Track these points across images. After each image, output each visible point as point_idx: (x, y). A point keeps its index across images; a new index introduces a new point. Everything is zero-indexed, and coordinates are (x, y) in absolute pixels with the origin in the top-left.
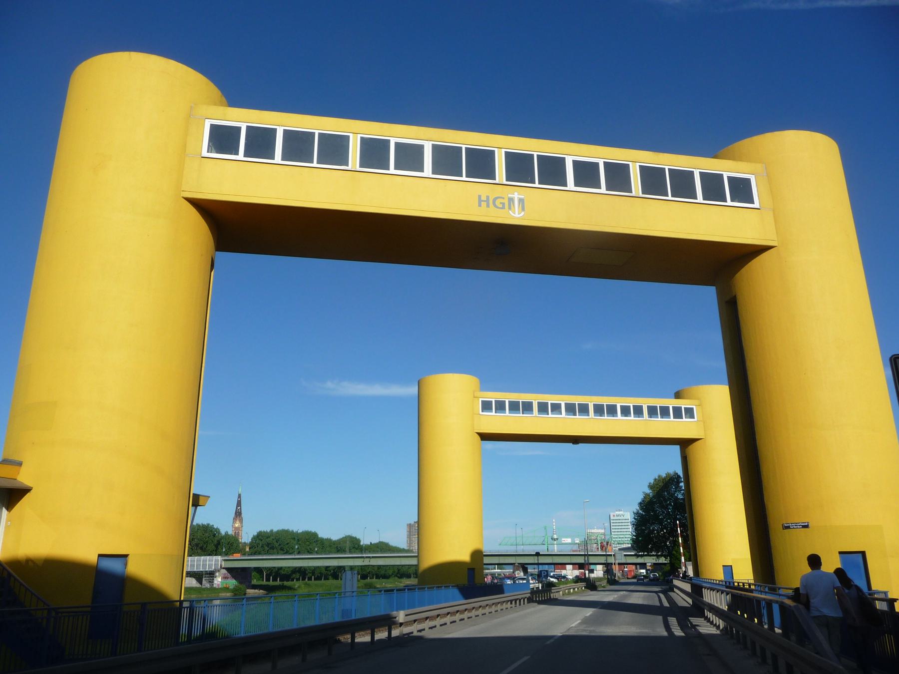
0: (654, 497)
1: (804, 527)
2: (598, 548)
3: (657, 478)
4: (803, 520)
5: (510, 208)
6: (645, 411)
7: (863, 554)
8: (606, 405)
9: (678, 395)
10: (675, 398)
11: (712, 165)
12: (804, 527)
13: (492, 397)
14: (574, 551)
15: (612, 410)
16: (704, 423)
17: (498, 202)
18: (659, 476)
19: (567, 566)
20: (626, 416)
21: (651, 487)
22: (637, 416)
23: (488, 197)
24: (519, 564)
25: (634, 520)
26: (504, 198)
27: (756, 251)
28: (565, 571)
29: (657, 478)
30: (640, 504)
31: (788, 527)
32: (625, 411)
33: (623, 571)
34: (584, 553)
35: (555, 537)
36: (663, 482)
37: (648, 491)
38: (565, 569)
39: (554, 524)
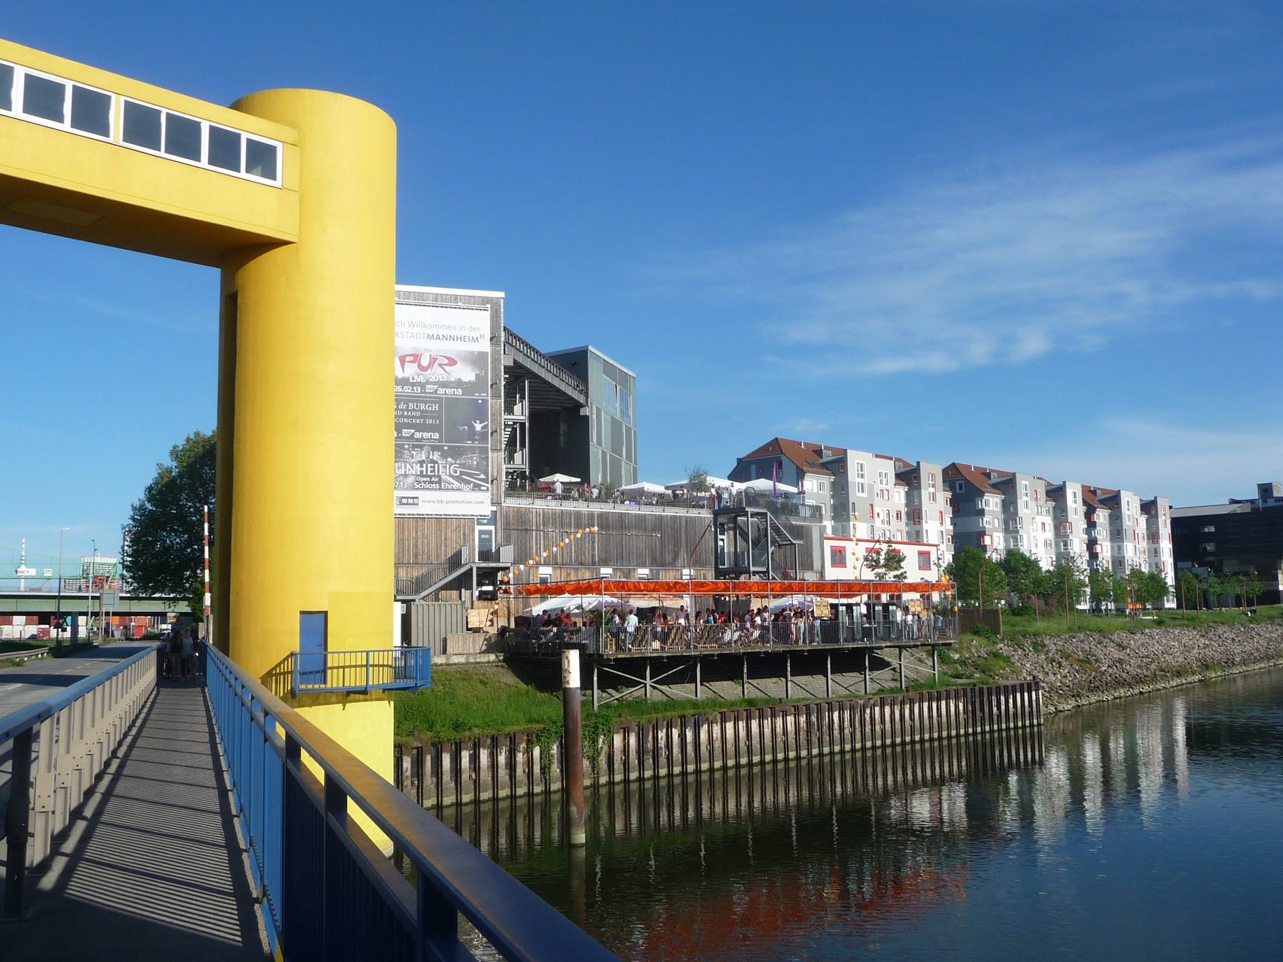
0: (180, 475)
2: (88, 587)
3: (192, 436)
6: (117, 116)
14: (32, 590)
16: (301, 198)
18: (197, 434)
19: (14, 617)
21: (175, 453)
25: (131, 522)
28: (11, 626)
29: (192, 436)
30: (150, 489)
33: (125, 627)
34: (57, 594)
36: (204, 446)
37: (170, 463)
38: (10, 623)
39: (24, 546)
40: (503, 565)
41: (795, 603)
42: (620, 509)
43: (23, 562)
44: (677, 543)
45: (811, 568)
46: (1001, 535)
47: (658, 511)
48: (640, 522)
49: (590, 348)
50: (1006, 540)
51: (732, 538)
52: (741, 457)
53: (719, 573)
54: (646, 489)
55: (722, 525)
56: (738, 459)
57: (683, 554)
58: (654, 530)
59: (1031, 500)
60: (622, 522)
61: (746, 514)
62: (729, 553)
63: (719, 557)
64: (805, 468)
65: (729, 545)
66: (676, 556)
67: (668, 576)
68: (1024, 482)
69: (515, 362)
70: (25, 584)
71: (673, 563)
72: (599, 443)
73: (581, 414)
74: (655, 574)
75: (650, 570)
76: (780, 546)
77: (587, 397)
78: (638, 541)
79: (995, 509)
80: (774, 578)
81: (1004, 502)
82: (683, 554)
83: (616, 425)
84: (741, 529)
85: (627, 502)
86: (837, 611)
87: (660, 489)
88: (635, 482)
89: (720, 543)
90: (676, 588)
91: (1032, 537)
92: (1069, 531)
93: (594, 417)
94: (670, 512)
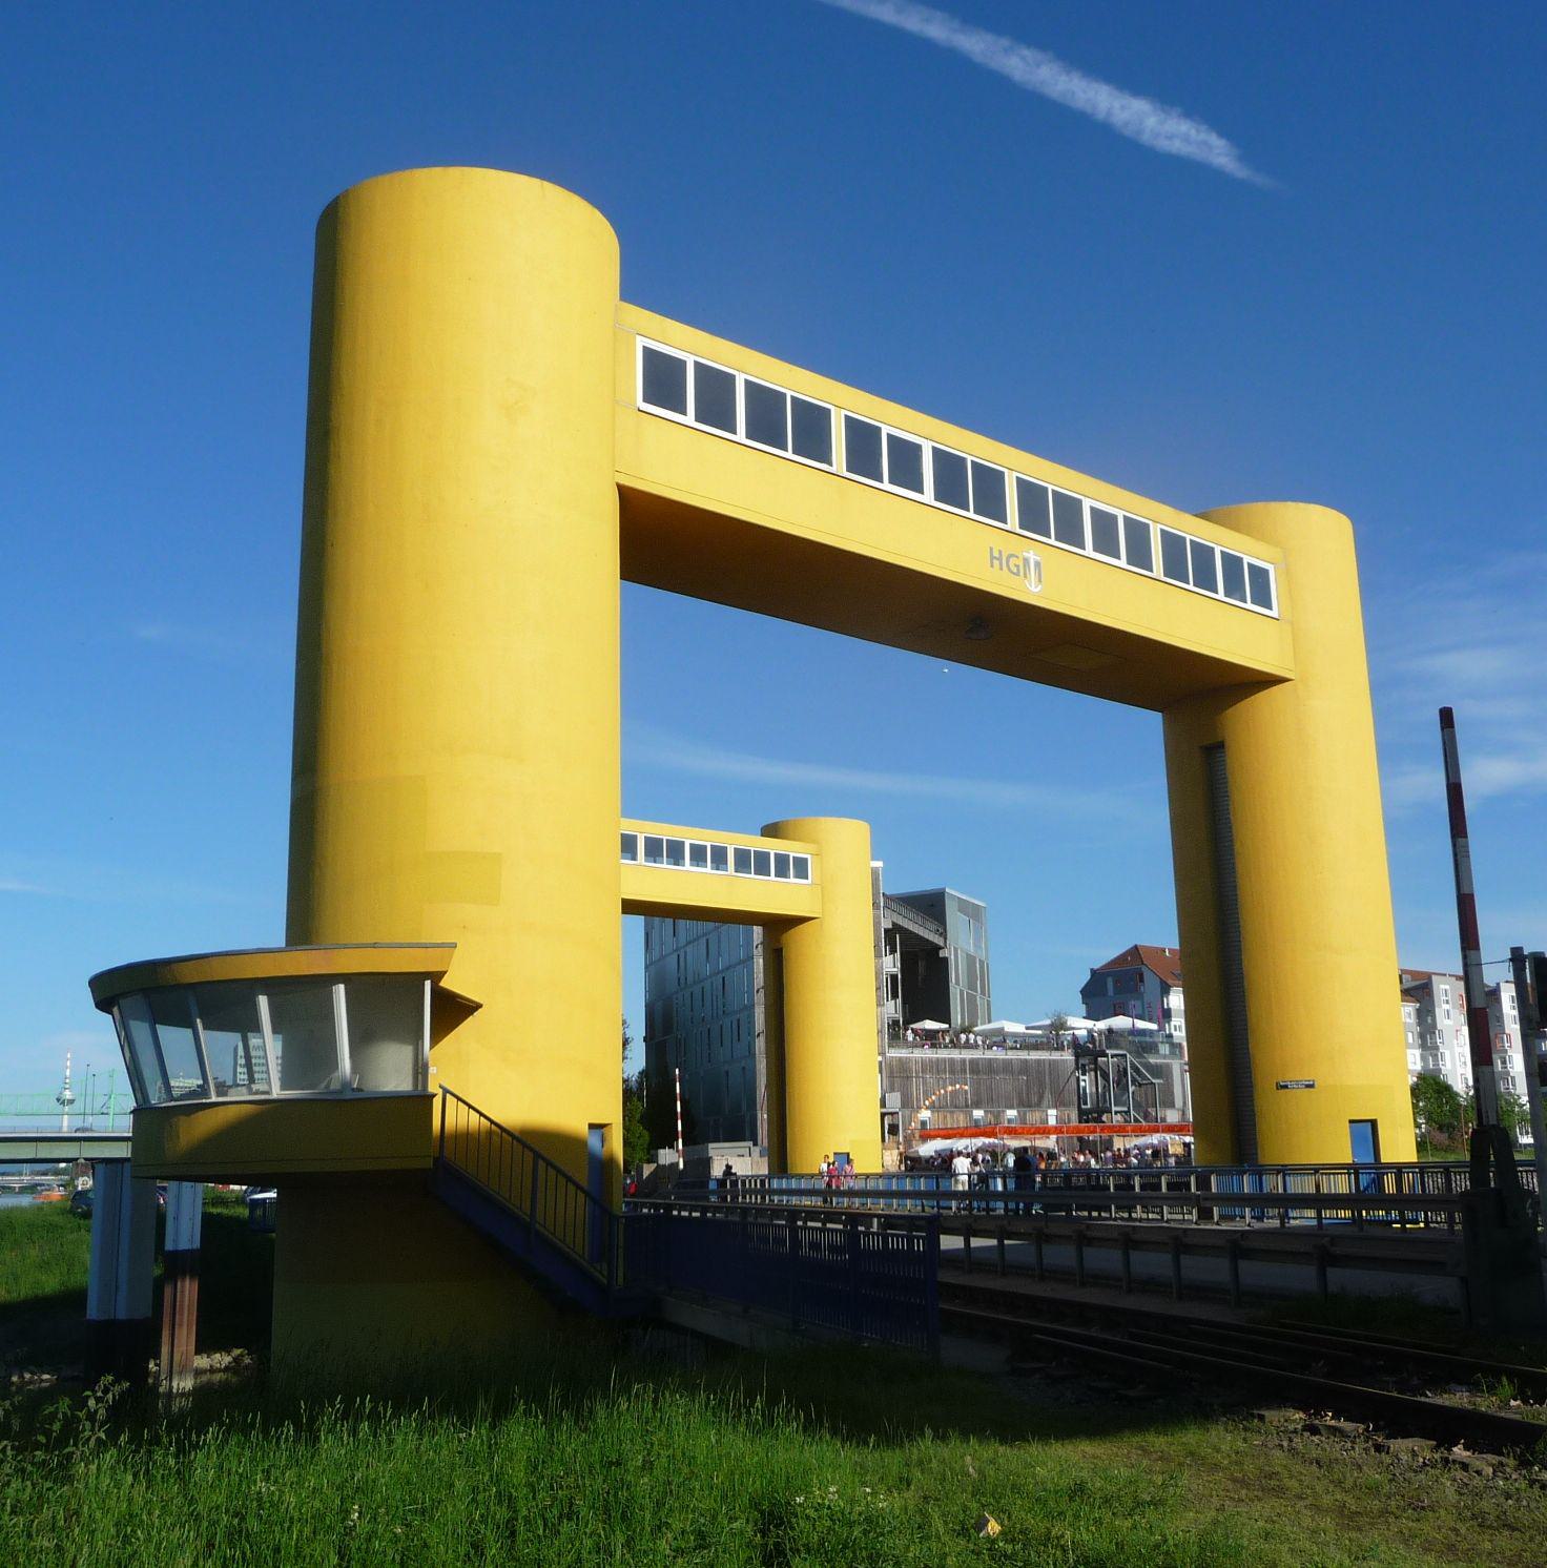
1: (1308, 1086)
4: (1306, 1077)
5: (1025, 576)
7: (1374, 1123)
8: (667, 840)
9: (771, 831)
10: (762, 835)
11: (1193, 529)
12: (1308, 1086)
13: (643, 830)
15: (675, 852)
16: (822, 888)
17: (1013, 561)
20: (676, 863)
22: (695, 863)
23: (1000, 552)
24: (86, 1159)
26: (1017, 557)
27: (1266, 681)
31: (1286, 1087)
32: (698, 854)
35: (68, 1095)
39: (68, 1064)
40: (890, 1110)
41: (1155, 1142)
42: (989, 1055)
43: (67, 1086)
44: (1042, 1085)
45: (1172, 1106)
46: (1418, 1052)
47: (1023, 1055)
48: (1007, 1066)
49: (947, 890)
50: (1424, 1058)
51: (1093, 1077)
52: (1096, 967)
53: (1081, 1113)
54: (1006, 1029)
55: (1084, 1066)
56: (1092, 970)
57: (1048, 1095)
58: (1020, 1073)
59: (1453, 1008)
60: (990, 1067)
61: (1106, 1056)
62: (1091, 1094)
63: (1081, 1097)
64: (1170, 982)
65: (1090, 1086)
66: (1041, 1098)
67: (1033, 1117)
68: (1442, 987)
69: (894, 924)
70: (69, 1122)
71: (1039, 1104)
72: (957, 983)
73: (941, 955)
74: (1022, 1118)
75: (1018, 1112)
76: (1140, 1085)
77: (945, 939)
78: (1005, 1084)
79: (1408, 1020)
80: (1136, 1120)
81: (1419, 1012)
82: (1048, 1095)
83: (971, 960)
84: (1101, 1069)
85: (995, 1048)
86: (1190, 1148)
87: (1019, 1028)
88: (989, 1022)
89: (1082, 1084)
90: (1045, 1131)
91: (1457, 1055)
92: (1506, 1045)
93: (953, 957)
94: (1035, 1055)
